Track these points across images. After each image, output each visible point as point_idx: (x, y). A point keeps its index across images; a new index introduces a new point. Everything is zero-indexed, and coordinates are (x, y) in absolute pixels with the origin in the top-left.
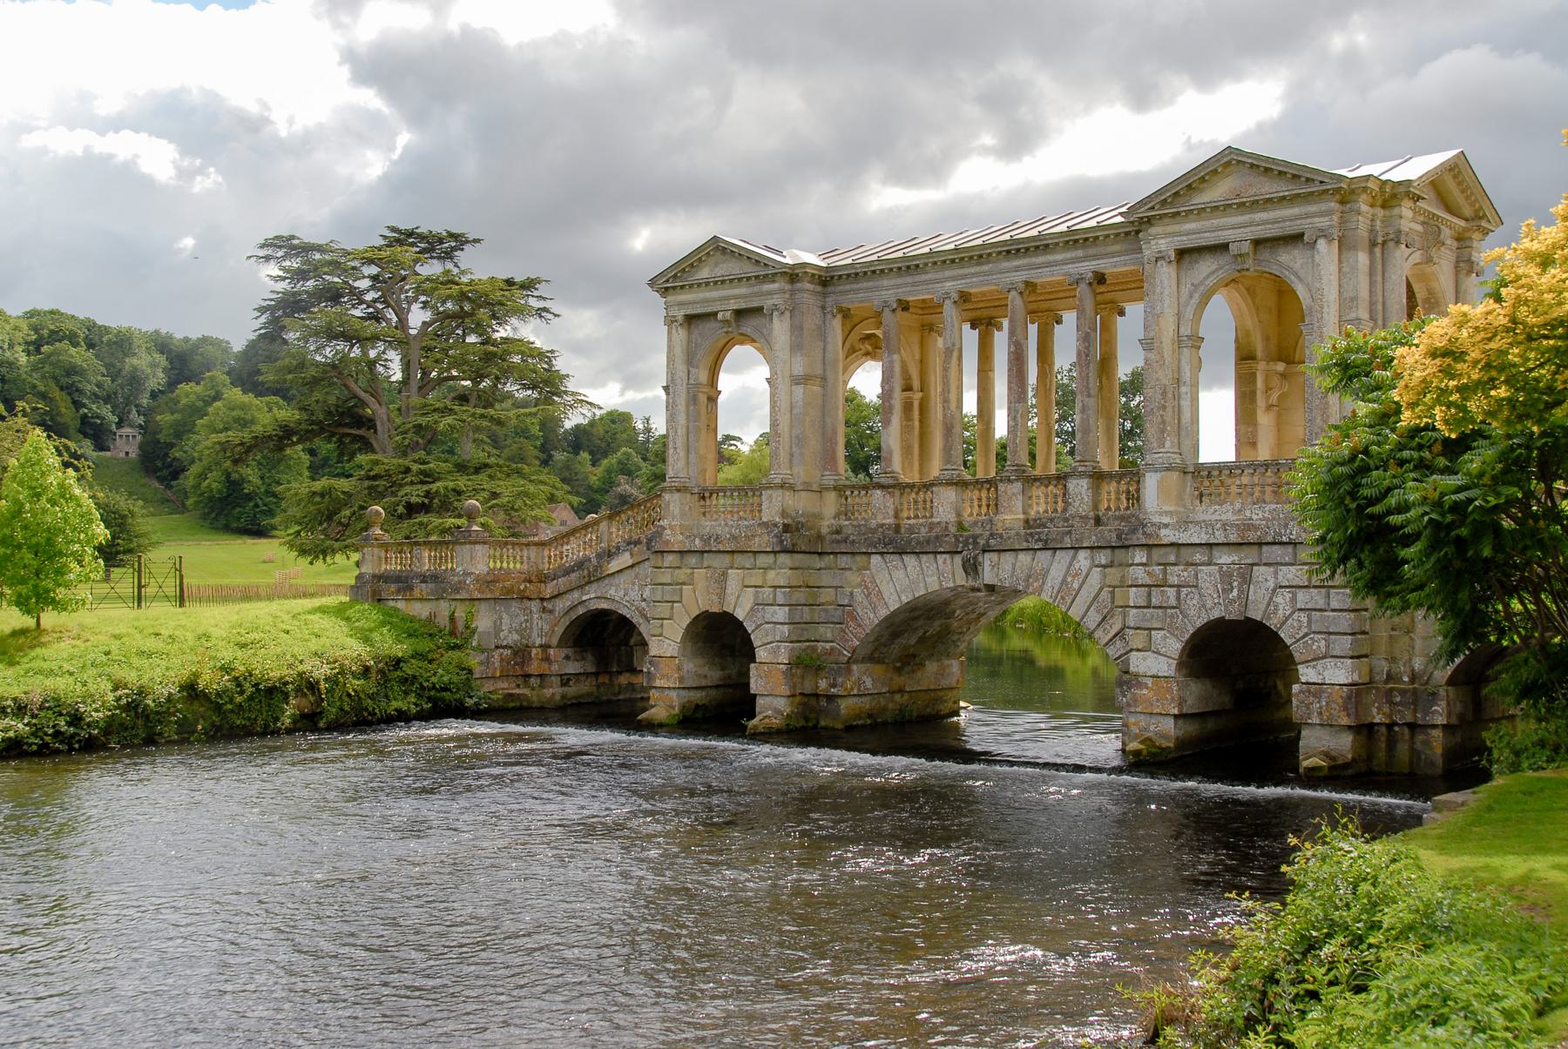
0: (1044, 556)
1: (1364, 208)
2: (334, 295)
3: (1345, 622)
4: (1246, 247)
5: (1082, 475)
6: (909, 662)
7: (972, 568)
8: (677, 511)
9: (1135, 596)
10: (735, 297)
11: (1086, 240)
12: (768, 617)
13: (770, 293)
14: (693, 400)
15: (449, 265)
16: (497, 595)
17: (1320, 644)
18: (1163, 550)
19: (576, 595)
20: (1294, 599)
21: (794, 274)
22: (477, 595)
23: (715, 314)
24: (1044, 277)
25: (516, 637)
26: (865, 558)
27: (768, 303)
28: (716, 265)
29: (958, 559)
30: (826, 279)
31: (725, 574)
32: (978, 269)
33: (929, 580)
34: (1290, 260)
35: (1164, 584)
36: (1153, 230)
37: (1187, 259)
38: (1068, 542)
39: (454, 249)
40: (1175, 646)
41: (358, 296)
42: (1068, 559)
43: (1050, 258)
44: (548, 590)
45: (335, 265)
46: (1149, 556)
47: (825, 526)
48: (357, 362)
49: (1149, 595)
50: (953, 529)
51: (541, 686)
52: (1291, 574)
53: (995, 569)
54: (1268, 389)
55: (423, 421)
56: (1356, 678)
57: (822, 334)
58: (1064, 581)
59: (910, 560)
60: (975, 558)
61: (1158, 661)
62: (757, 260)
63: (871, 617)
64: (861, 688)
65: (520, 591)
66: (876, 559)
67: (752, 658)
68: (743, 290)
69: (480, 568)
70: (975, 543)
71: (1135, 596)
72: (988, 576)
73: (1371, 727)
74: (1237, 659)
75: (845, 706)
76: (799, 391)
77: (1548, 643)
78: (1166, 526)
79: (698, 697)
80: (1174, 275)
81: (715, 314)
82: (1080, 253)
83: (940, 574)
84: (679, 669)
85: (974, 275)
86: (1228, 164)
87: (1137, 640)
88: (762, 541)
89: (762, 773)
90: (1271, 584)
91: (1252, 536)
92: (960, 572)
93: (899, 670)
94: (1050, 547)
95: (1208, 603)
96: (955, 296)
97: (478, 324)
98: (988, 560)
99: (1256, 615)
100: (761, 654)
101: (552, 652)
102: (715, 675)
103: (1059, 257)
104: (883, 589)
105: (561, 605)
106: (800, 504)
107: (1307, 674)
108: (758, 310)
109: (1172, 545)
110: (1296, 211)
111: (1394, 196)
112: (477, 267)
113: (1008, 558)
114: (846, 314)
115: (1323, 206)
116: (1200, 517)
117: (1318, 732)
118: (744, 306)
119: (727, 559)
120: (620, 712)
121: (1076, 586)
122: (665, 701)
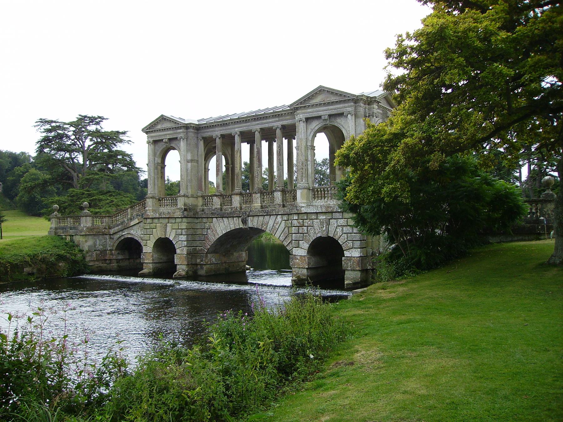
1: (362, 105)
2: (60, 137)
3: (358, 236)
4: (327, 117)
5: (279, 191)
6: (227, 253)
7: (244, 222)
8: (151, 205)
9: (294, 230)
10: (169, 134)
11: (279, 115)
12: (180, 239)
13: (179, 133)
14: (156, 168)
15: (98, 127)
16: (95, 233)
17: (350, 244)
18: (302, 215)
19: (121, 233)
20: (342, 230)
21: (187, 127)
25: (101, 247)
26: (211, 219)
27: (179, 136)
28: (163, 124)
29: (240, 219)
30: (198, 128)
31: (166, 225)
32: (245, 124)
33: (231, 226)
34: (339, 122)
36: (298, 112)
37: (309, 121)
39: (100, 121)
40: (306, 246)
41: (68, 137)
42: (274, 218)
43: (268, 121)
44: (112, 231)
45: (59, 127)
47: (200, 208)
48: (67, 158)
49: (299, 229)
50: (239, 209)
51: (110, 263)
52: (341, 222)
53: (253, 223)
55: (88, 177)
57: (197, 146)
58: (273, 225)
59: (225, 220)
60: (246, 218)
61: (300, 252)
62: (175, 122)
63: (213, 238)
65: (103, 232)
66: (214, 219)
68: (171, 132)
70: (246, 213)
71: (294, 230)
72: (250, 225)
73: (367, 270)
74: (326, 251)
76: (189, 164)
78: (303, 207)
80: (305, 126)
82: (277, 119)
83: (234, 224)
85: (244, 126)
86: (320, 91)
88: (178, 214)
89: (186, 290)
90: (336, 225)
91: (329, 210)
93: (224, 256)
95: (317, 230)
96: (238, 133)
97: (107, 146)
98: (250, 219)
99: (331, 235)
100: (178, 251)
101: (113, 252)
102: (164, 258)
103: (270, 120)
104: (217, 229)
106: (190, 201)
107: (347, 254)
109: (305, 213)
110: (341, 106)
111: (371, 102)
112: (106, 127)
113: (256, 218)
115: (350, 104)
116: (314, 204)
117: (350, 272)
118: (171, 137)
119: (167, 220)
121: (277, 227)
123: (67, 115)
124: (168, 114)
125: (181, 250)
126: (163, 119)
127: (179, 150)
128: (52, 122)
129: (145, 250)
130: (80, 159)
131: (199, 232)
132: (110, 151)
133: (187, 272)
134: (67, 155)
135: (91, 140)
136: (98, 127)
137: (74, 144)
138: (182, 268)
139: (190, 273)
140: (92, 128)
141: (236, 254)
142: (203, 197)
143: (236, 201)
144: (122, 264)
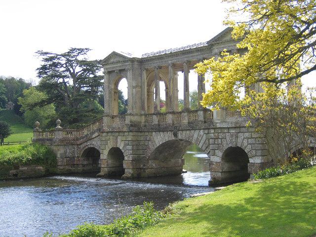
0: (193, 131)
7: (175, 135)
21: (133, 60)
22: (59, 144)
23: (115, 71)
24: (190, 59)
30: (142, 62)
33: (166, 138)
35: (218, 138)
36: (214, 47)
38: (198, 128)
46: (215, 131)
52: (247, 135)
56: (263, 161)
57: (141, 75)
64: (153, 166)
66: (154, 133)
69: (61, 137)
72: (180, 137)
76: (134, 90)
79: (113, 169)
81: (115, 71)
84: (107, 162)
88: (125, 129)
90: (243, 137)
91: (238, 125)
94: (194, 129)
95: (228, 142)
98: (179, 133)
99: (239, 145)
100: (126, 158)
103: (195, 54)
105: (82, 146)
106: (135, 119)
107: (251, 161)
108: (124, 70)
113: (184, 132)
114: (147, 70)
120: (93, 172)
122: (104, 169)
123: (59, 48)
124: (118, 51)
125: (128, 158)
126: (114, 54)
127: (127, 78)
128: (46, 53)
130: (70, 82)
131: (142, 143)
133: (132, 175)
138: (129, 171)
139: (135, 175)
140: (80, 58)
141: (173, 161)
142: (146, 115)
144: (85, 168)
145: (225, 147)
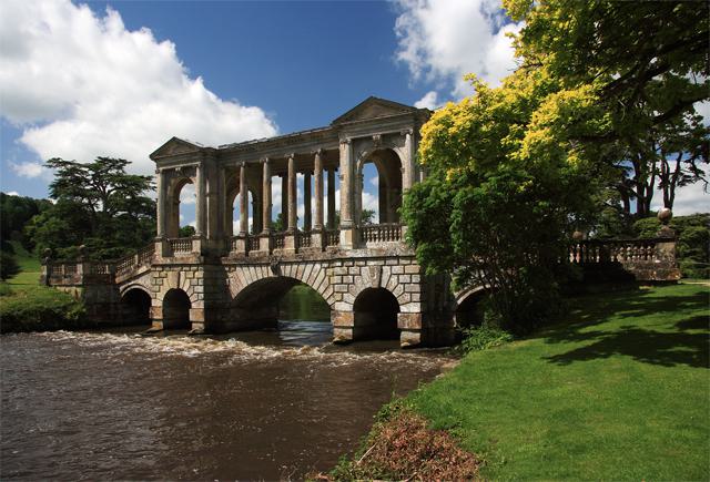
0: (302, 267)
7: (276, 270)
15: (120, 171)
25: (103, 300)
35: (348, 274)
40: (352, 299)
41: (87, 182)
48: (86, 204)
52: (397, 269)
53: (287, 271)
54: (391, 199)
61: (344, 307)
67: (190, 307)
72: (343, 233)
75: (229, 324)
77: (641, 60)
87: (338, 297)
91: (382, 254)
92: (270, 271)
107: (403, 309)
126: (175, 142)
129: (154, 303)
132: (133, 197)
134: (86, 201)
135: (112, 185)
136: (120, 171)
137: (95, 189)
143: (264, 243)
145: (360, 287)
